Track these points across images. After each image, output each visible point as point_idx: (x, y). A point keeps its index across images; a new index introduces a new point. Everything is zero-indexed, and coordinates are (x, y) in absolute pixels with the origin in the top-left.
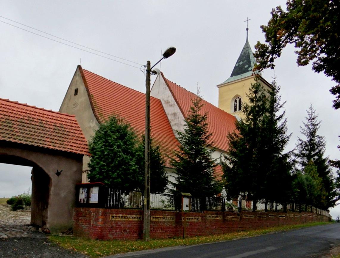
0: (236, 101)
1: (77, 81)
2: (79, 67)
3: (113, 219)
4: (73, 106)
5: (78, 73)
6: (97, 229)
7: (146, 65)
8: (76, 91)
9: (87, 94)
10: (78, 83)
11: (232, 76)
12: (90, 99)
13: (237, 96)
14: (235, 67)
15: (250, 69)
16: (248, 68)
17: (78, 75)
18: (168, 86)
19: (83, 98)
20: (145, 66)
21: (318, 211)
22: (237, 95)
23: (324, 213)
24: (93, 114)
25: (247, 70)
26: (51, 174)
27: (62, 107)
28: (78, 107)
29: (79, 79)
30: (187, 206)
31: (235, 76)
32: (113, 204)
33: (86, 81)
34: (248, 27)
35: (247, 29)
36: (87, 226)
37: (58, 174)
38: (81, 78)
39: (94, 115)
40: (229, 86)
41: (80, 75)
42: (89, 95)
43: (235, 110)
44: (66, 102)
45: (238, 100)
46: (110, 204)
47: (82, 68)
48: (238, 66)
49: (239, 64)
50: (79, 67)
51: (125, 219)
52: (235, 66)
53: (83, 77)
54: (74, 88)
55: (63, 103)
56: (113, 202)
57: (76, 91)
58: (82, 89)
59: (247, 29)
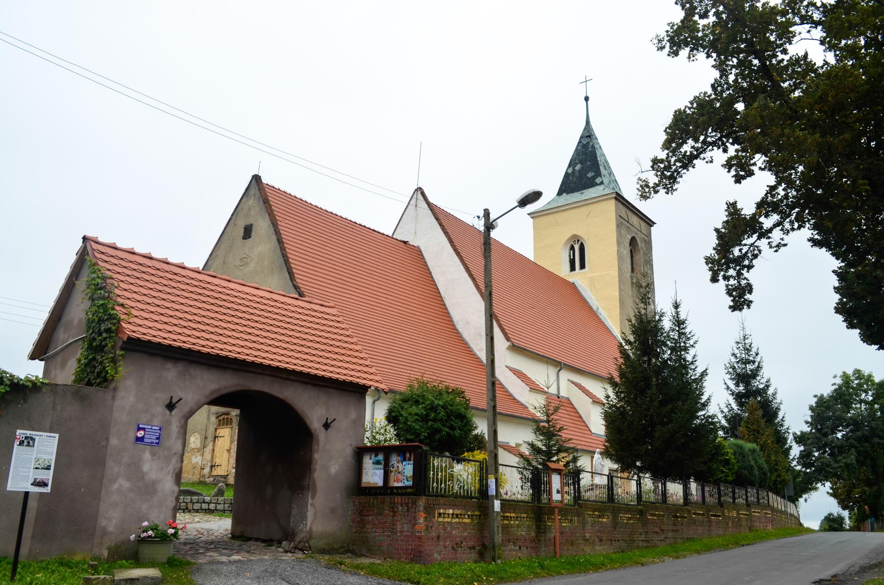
0: (572, 248)
1: (250, 209)
2: (256, 179)
3: (441, 519)
4: (238, 263)
5: (254, 190)
6: (413, 541)
7: (481, 214)
8: (248, 232)
9: (274, 237)
10: (253, 213)
11: (560, 193)
12: (283, 249)
13: (576, 239)
14: (567, 175)
15: (598, 180)
16: (594, 178)
17: (254, 195)
18: (437, 219)
19: (263, 245)
20: (479, 217)
21: (777, 501)
22: (574, 236)
23: (791, 508)
24: (290, 283)
25: (591, 184)
26: (315, 422)
27: (210, 263)
28: (252, 265)
29: (253, 202)
30: (558, 492)
31: (568, 193)
32: (437, 488)
33: (272, 210)
34: (168, 412)
35: (587, 99)
36: (389, 536)
37: (327, 426)
38: (261, 202)
39: (294, 285)
40: (555, 215)
41: (258, 195)
42: (280, 241)
43: (573, 268)
44: (221, 252)
45: (577, 247)
46: (433, 488)
47: (264, 181)
48: (573, 172)
49: (574, 169)
50: (256, 179)
51: (457, 520)
52: (566, 172)
53: (266, 201)
54: (241, 224)
55: (211, 254)
56: (437, 483)
57: (248, 232)
58: (262, 226)
59: (587, 99)
